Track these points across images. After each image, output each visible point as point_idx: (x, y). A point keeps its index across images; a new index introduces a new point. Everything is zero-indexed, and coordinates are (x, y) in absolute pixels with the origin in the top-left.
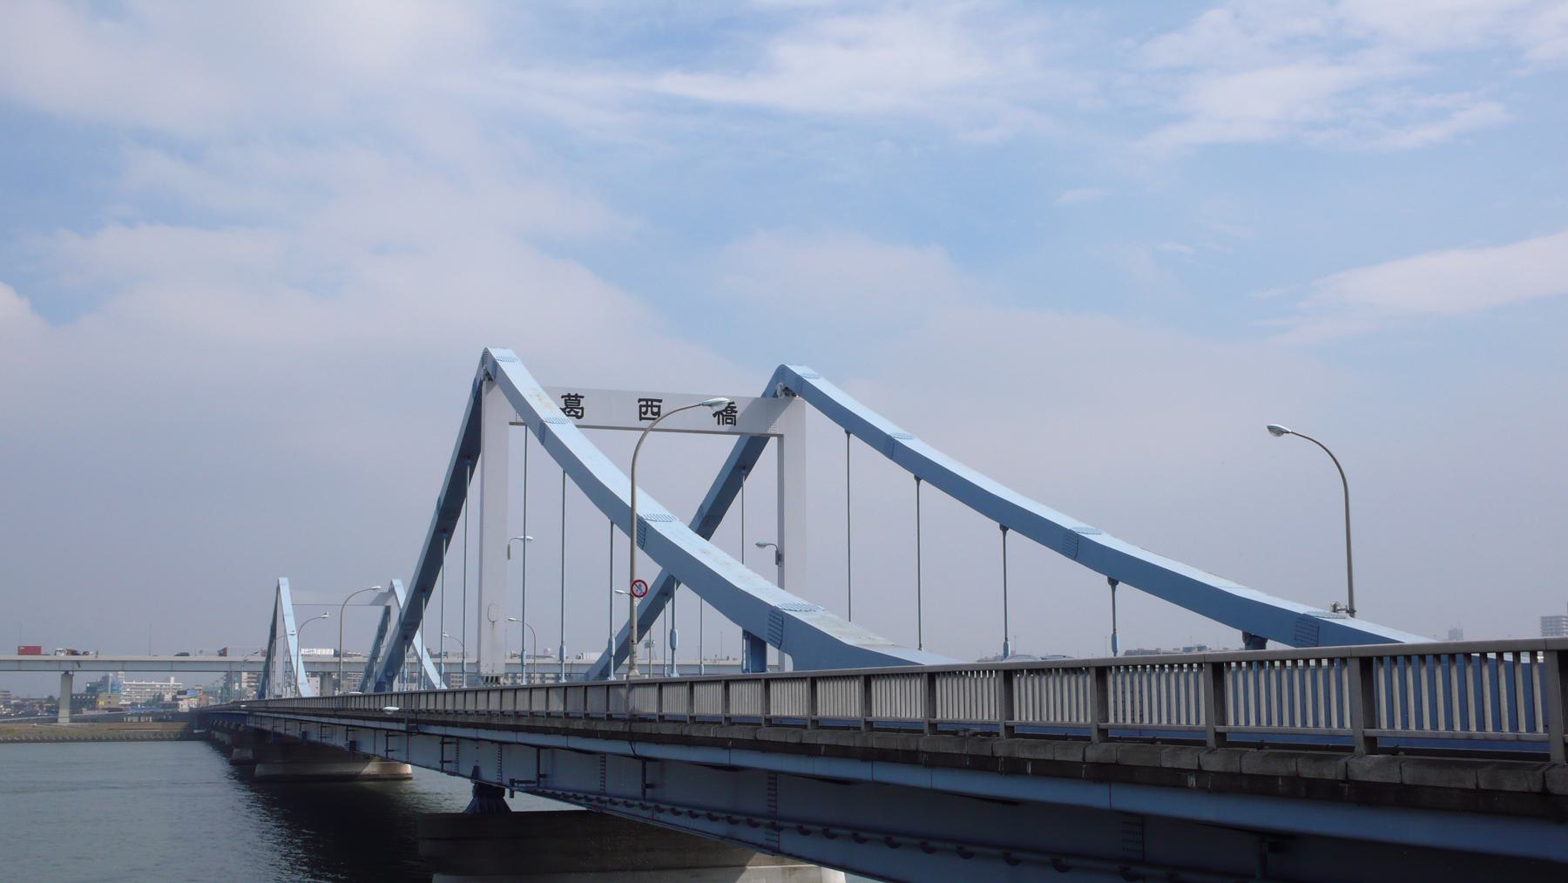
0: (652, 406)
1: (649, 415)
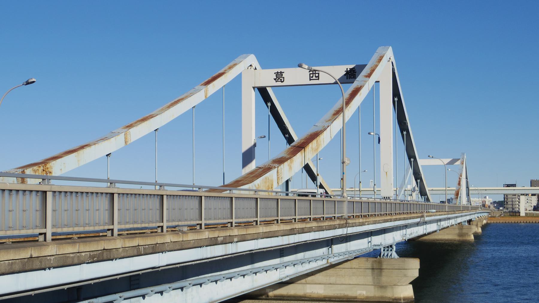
0: (315, 73)
1: (314, 78)
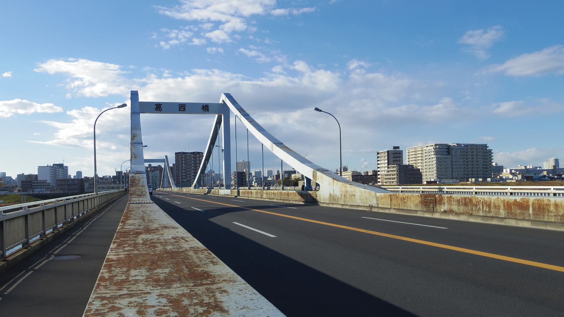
0: (183, 107)
1: (182, 109)
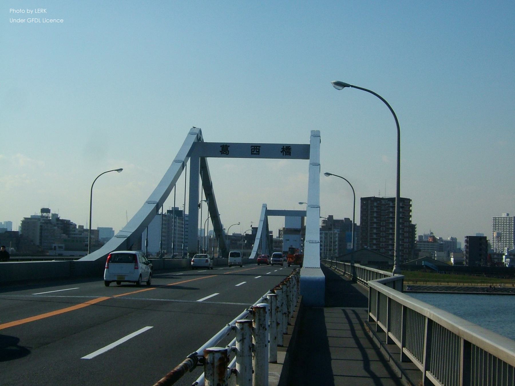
0: (257, 149)
